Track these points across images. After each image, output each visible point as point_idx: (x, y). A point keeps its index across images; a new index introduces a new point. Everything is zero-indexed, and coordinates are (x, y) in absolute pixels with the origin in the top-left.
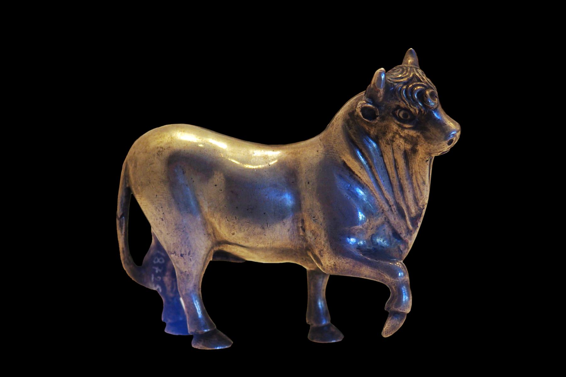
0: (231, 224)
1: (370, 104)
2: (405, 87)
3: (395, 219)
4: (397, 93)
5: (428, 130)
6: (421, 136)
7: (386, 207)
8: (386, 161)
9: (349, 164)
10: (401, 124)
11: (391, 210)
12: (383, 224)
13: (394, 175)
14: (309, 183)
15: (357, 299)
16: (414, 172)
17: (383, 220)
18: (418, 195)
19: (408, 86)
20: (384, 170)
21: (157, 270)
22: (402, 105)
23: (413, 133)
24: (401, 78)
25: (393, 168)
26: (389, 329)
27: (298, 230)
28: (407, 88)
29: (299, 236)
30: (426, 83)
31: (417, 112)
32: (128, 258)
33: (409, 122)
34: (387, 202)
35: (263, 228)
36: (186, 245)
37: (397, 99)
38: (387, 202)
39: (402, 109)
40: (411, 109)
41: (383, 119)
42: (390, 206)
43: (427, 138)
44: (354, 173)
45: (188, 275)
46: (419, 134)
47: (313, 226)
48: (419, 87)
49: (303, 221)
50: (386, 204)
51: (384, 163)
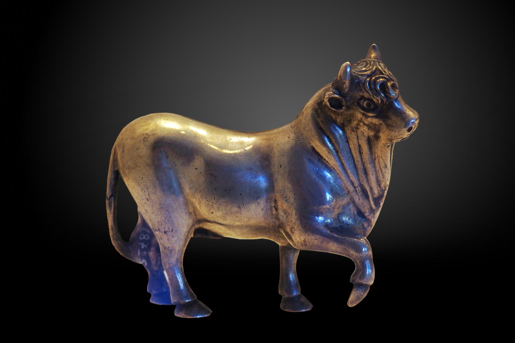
0: (211, 204)
1: (337, 94)
2: (368, 79)
3: (359, 199)
4: (361, 85)
5: (389, 118)
6: (383, 124)
7: (351, 189)
8: (352, 146)
9: (318, 149)
10: (365, 113)
11: (356, 191)
12: (348, 204)
13: (359, 159)
14: (281, 166)
15: (325, 273)
16: (376, 156)
17: (349, 200)
18: (381, 178)
19: (371, 79)
20: (349, 155)
21: (143, 246)
22: (366, 95)
23: (375, 121)
24: (365, 71)
25: (358, 153)
26: (354, 299)
27: (271, 209)
28: (370, 80)
29: (272, 214)
30: (388, 75)
31: (380, 102)
32: (116, 235)
33: (372, 111)
34: (352, 184)
35: (240, 208)
36: (169, 223)
37: (361, 90)
38: (352, 184)
39: (365, 99)
40: (374, 100)
41: (348, 108)
42: (355, 188)
43: (388, 126)
44: (322, 157)
45: (171, 251)
46: (381, 122)
47: (285, 206)
48: (381, 80)
49: (276, 201)
50: (351, 185)
51: (350, 148)
